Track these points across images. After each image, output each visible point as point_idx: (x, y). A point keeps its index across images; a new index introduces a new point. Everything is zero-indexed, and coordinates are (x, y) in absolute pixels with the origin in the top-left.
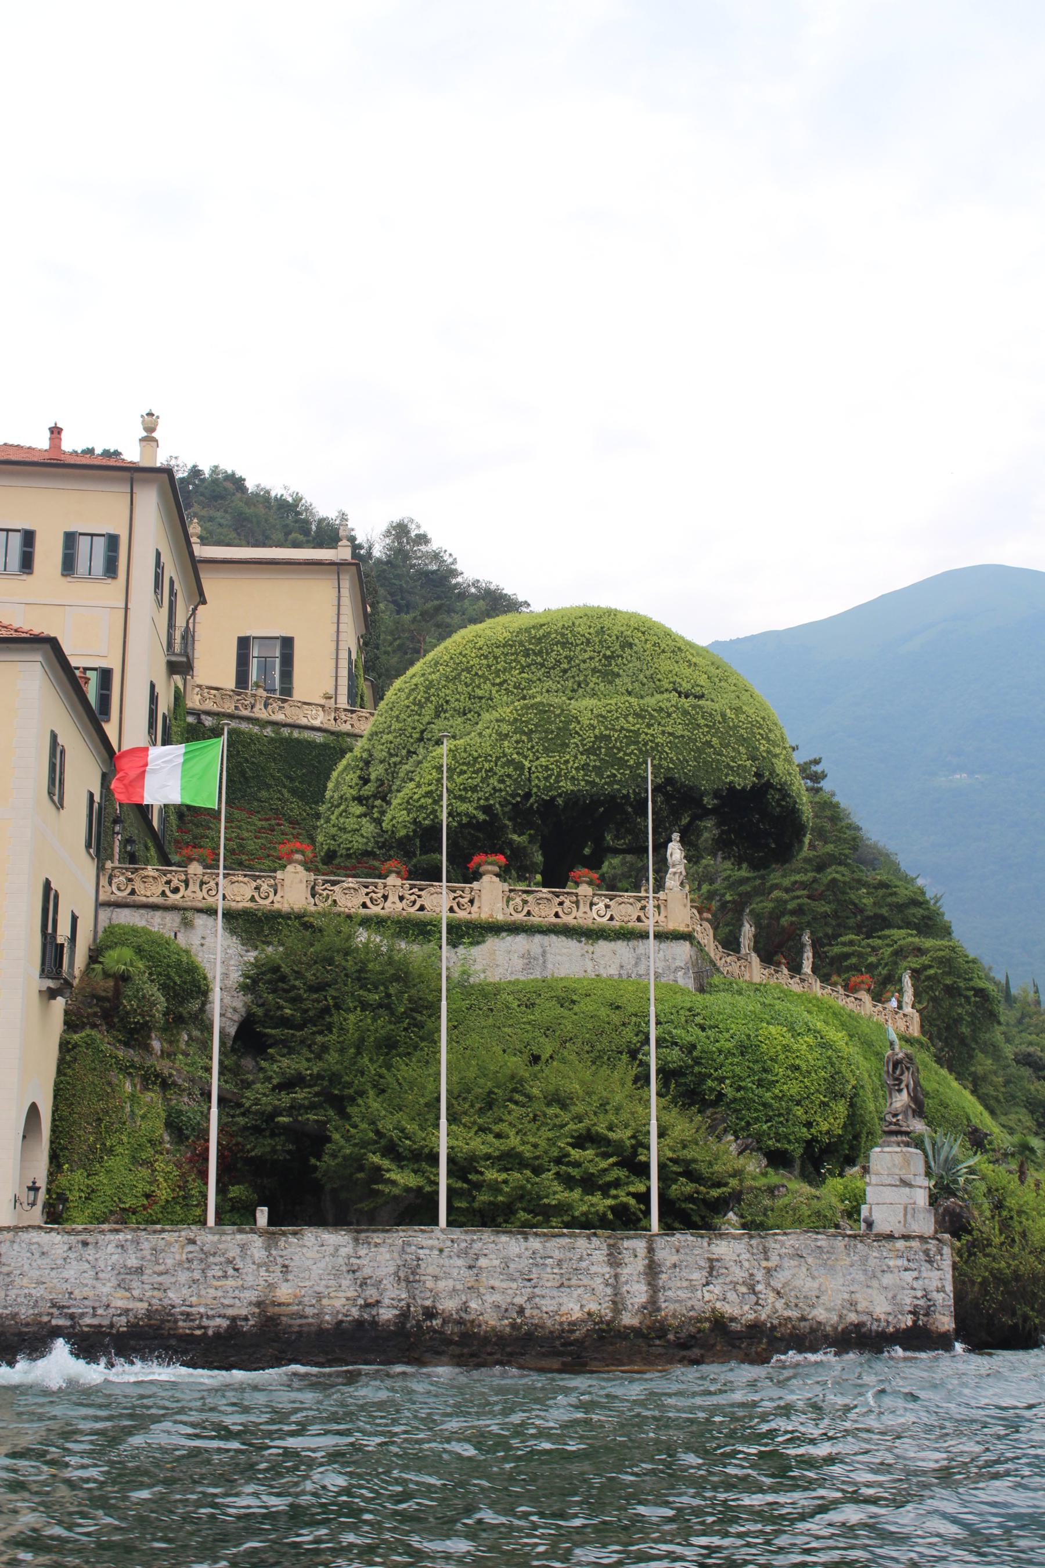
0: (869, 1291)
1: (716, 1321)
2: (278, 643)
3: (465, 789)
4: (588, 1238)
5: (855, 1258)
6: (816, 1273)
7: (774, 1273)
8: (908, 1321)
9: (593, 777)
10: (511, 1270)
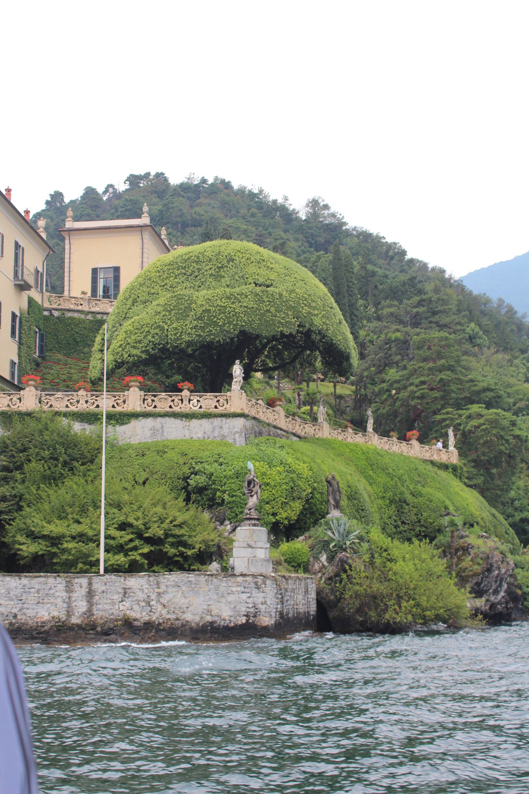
0: (220, 604)
1: (126, 621)
2: (112, 269)
3: (136, 342)
4: (55, 577)
6: (187, 595)
7: (163, 595)
8: (244, 620)
9: (200, 332)
10: (11, 595)
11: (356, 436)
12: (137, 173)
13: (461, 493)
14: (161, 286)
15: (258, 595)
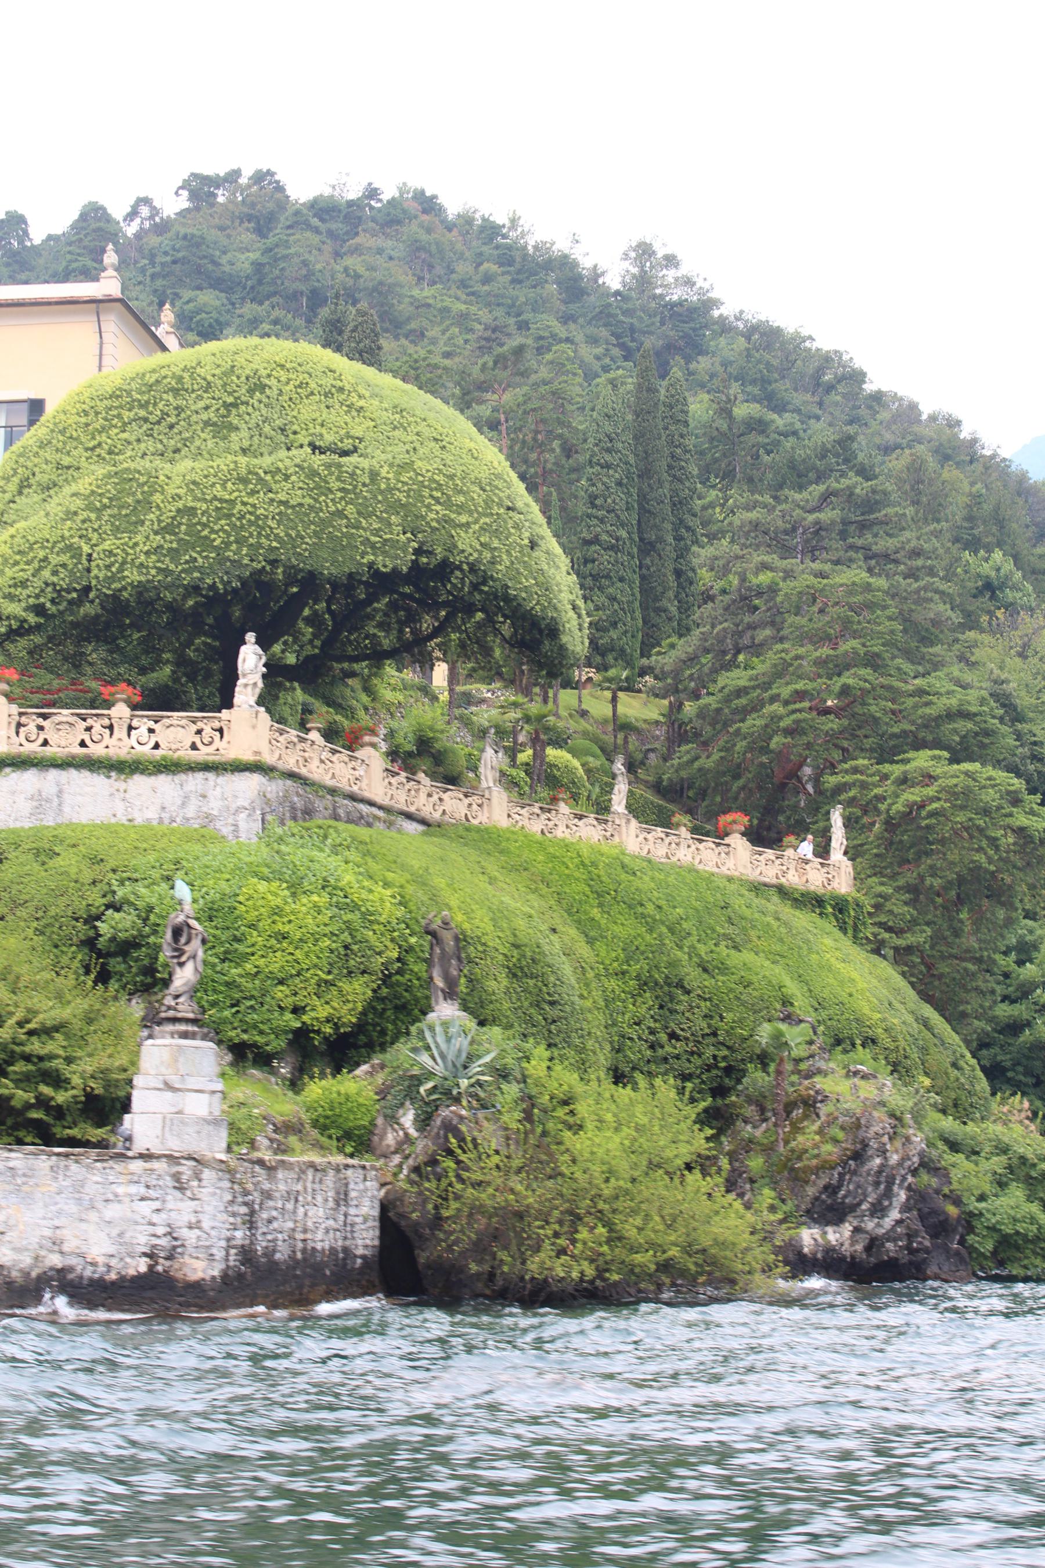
0: (84, 1226)
2: (26, 406)
3: (15, 586)
5: (64, 1183)
8: (142, 1266)
11: (581, 823)
12: (208, 171)
13: (840, 965)
14: (87, 449)
15: (181, 1205)
